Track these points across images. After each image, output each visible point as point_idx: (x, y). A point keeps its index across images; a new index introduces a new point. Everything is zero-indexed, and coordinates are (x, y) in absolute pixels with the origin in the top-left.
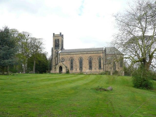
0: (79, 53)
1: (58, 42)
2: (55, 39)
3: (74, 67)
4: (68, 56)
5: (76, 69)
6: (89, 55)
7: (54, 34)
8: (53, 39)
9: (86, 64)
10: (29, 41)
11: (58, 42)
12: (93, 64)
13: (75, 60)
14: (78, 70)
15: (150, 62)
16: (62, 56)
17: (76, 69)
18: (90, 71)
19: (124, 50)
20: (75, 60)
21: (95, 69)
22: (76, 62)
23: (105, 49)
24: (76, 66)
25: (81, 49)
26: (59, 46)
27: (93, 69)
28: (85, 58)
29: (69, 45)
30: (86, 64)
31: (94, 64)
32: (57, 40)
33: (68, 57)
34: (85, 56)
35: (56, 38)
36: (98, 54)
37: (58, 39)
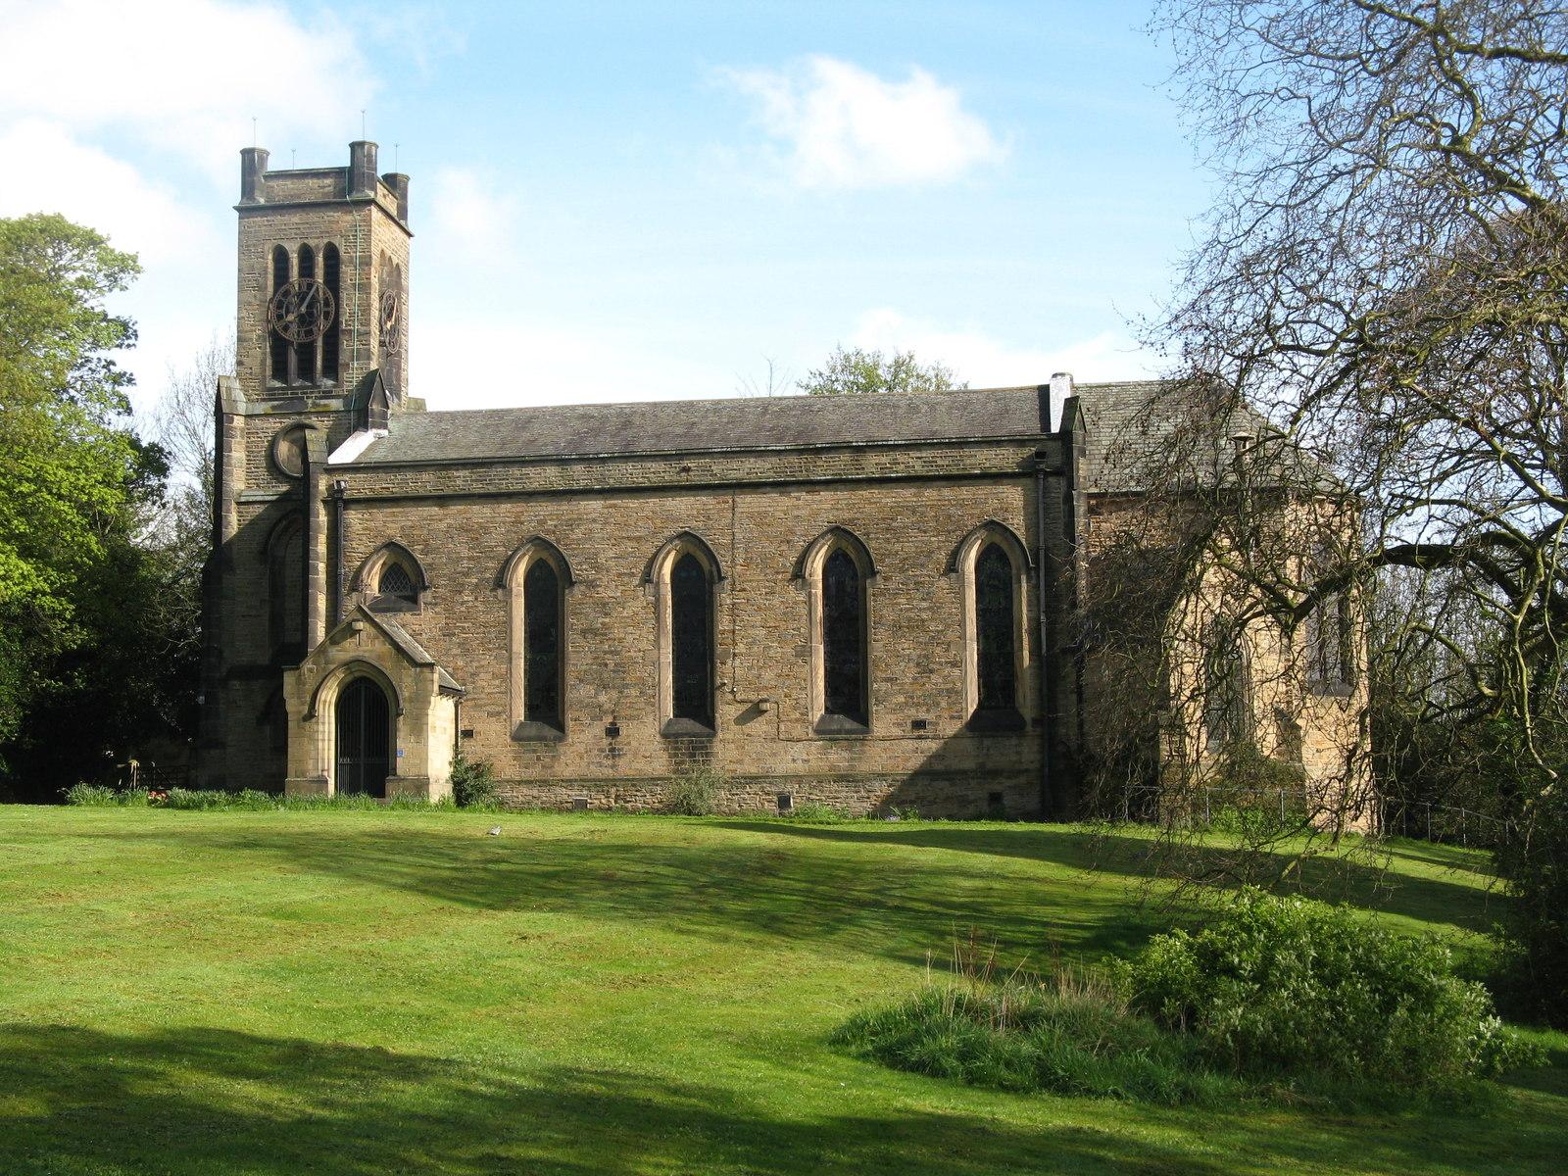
0: (654, 466)
1: (312, 314)
2: (281, 256)
3: (577, 693)
4: (480, 513)
5: (613, 731)
6: (828, 506)
7: (251, 160)
8: (244, 249)
9: (773, 644)
10: (1285, 129)
11: (312, 314)
12: (879, 644)
13: (591, 585)
14: (646, 746)
15: (101, 583)
16: (393, 523)
17: (613, 731)
18: (838, 757)
19: (1383, 442)
20: (591, 585)
21: (919, 725)
22: (604, 607)
23: (1071, 404)
24: (613, 674)
25: (690, 406)
26: (343, 358)
27: (883, 723)
28: (621, 556)
29: (483, 337)
30: (773, 644)
31: (906, 646)
32: (306, 255)
33: (474, 534)
34: (760, 519)
35: (293, 232)
36: (965, 492)
37: (318, 243)
